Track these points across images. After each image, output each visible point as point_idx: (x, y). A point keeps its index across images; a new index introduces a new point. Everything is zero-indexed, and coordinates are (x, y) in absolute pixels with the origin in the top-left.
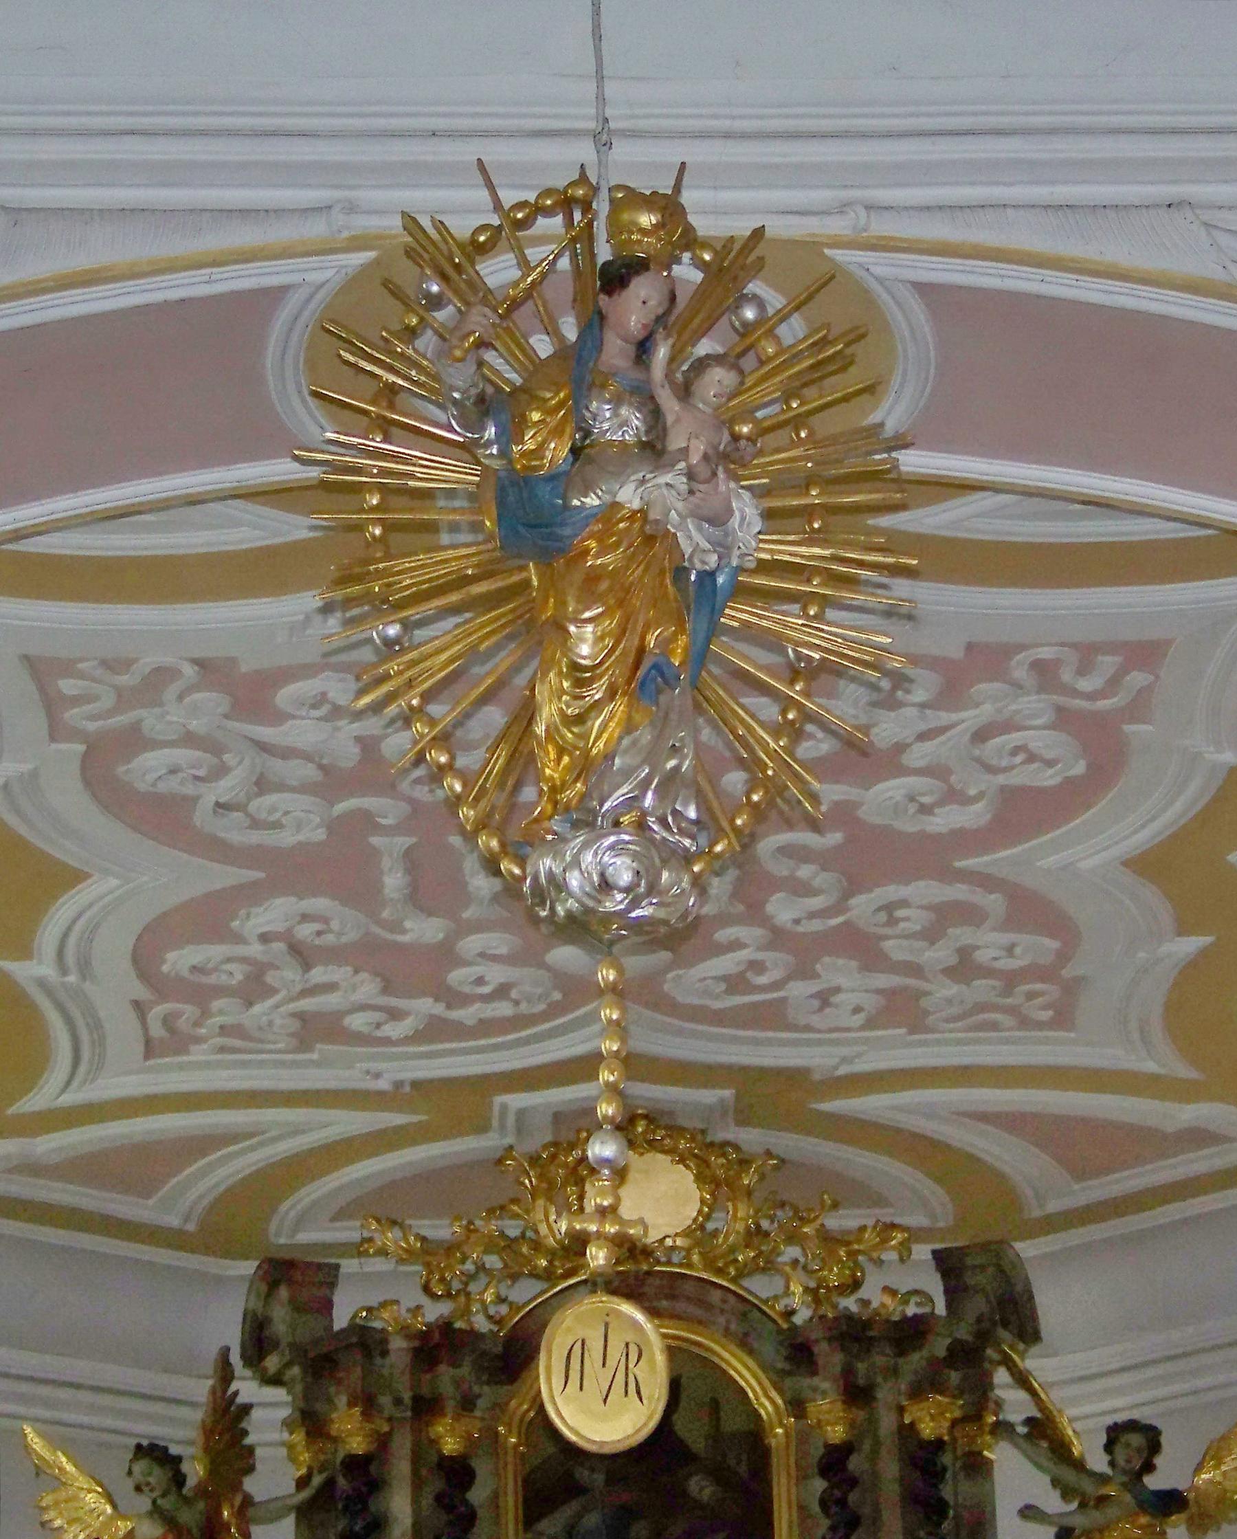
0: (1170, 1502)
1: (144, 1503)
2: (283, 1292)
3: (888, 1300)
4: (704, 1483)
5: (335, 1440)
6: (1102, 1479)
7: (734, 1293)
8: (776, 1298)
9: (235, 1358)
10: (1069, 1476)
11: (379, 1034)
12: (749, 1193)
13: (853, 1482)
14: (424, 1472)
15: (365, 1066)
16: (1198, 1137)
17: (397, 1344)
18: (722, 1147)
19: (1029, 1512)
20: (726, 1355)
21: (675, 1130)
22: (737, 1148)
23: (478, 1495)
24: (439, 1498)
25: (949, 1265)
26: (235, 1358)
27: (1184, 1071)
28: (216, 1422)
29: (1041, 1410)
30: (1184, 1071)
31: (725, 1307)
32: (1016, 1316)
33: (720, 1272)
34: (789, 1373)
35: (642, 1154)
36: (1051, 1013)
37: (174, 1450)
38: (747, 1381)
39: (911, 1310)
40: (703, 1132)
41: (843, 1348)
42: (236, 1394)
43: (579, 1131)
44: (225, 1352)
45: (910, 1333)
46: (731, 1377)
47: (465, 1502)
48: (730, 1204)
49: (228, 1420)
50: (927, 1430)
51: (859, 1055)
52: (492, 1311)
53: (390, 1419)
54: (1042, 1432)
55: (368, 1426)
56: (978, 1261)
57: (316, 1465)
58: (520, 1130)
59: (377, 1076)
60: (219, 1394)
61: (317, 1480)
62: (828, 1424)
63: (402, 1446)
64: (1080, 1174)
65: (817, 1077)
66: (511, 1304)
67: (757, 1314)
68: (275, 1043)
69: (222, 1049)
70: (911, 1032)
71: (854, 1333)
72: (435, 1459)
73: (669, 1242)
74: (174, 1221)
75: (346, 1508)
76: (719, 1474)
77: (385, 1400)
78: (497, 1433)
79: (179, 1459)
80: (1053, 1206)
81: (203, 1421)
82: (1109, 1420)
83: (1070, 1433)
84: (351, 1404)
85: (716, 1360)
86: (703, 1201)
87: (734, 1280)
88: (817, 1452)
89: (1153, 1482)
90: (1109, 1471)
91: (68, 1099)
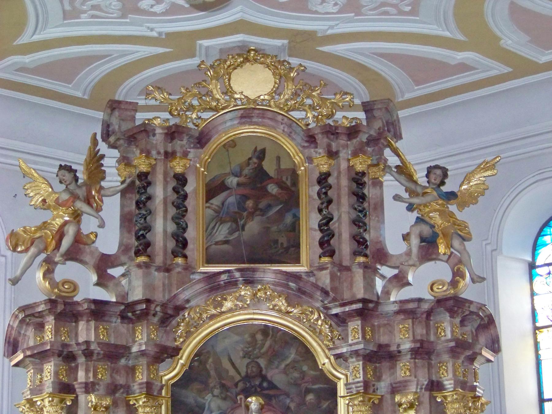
0: (451, 196)
1: (63, 187)
2: (116, 113)
3: (344, 121)
4: (274, 187)
5: (135, 167)
6: (425, 187)
7: (286, 116)
8: (302, 119)
9: (99, 137)
10: (412, 186)
11: (152, 10)
12: (293, 79)
13: (330, 187)
14: (168, 179)
15: (148, 25)
16: (463, 67)
17: (158, 131)
18: (282, 63)
19: (397, 198)
20: (283, 140)
21: (265, 56)
22: (289, 63)
23: (189, 189)
24: (174, 189)
25: (367, 108)
26: (99, 137)
27: (460, 37)
28: (91, 160)
29: (402, 163)
30: (460, 37)
31: (283, 122)
32: (392, 129)
33: (281, 109)
34: (307, 147)
35: (252, 64)
36: (410, 8)
37: (74, 167)
38: (289, 149)
39: (354, 124)
40: (276, 56)
41: (327, 137)
42: (99, 150)
43: (229, 55)
44: (95, 134)
45: (353, 132)
46: (285, 149)
47: (184, 190)
48: (286, 83)
49: (95, 161)
50: (359, 168)
51: (337, 25)
52: (195, 122)
53: (155, 159)
54: (403, 171)
55: (147, 161)
56: (379, 106)
57: (127, 176)
58: (207, 55)
59: (152, 30)
60: (92, 150)
61: (128, 181)
62: (322, 165)
63: (160, 170)
64: (418, 83)
65: (319, 35)
66: (202, 119)
67: (295, 125)
68: (112, 14)
69: (93, 17)
70: (356, 15)
71: (331, 132)
72: (172, 174)
73: (262, 97)
74: (79, 94)
75: (138, 192)
76: (280, 184)
77: (154, 153)
78: (196, 167)
79: (76, 171)
80: (408, 96)
81: (86, 160)
82: (428, 165)
83: (413, 170)
84: (141, 153)
85: (278, 142)
86: (275, 83)
87: (287, 112)
88: (316, 175)
89: (445, 189)
90: (427, 185)
91: (37, 38)
